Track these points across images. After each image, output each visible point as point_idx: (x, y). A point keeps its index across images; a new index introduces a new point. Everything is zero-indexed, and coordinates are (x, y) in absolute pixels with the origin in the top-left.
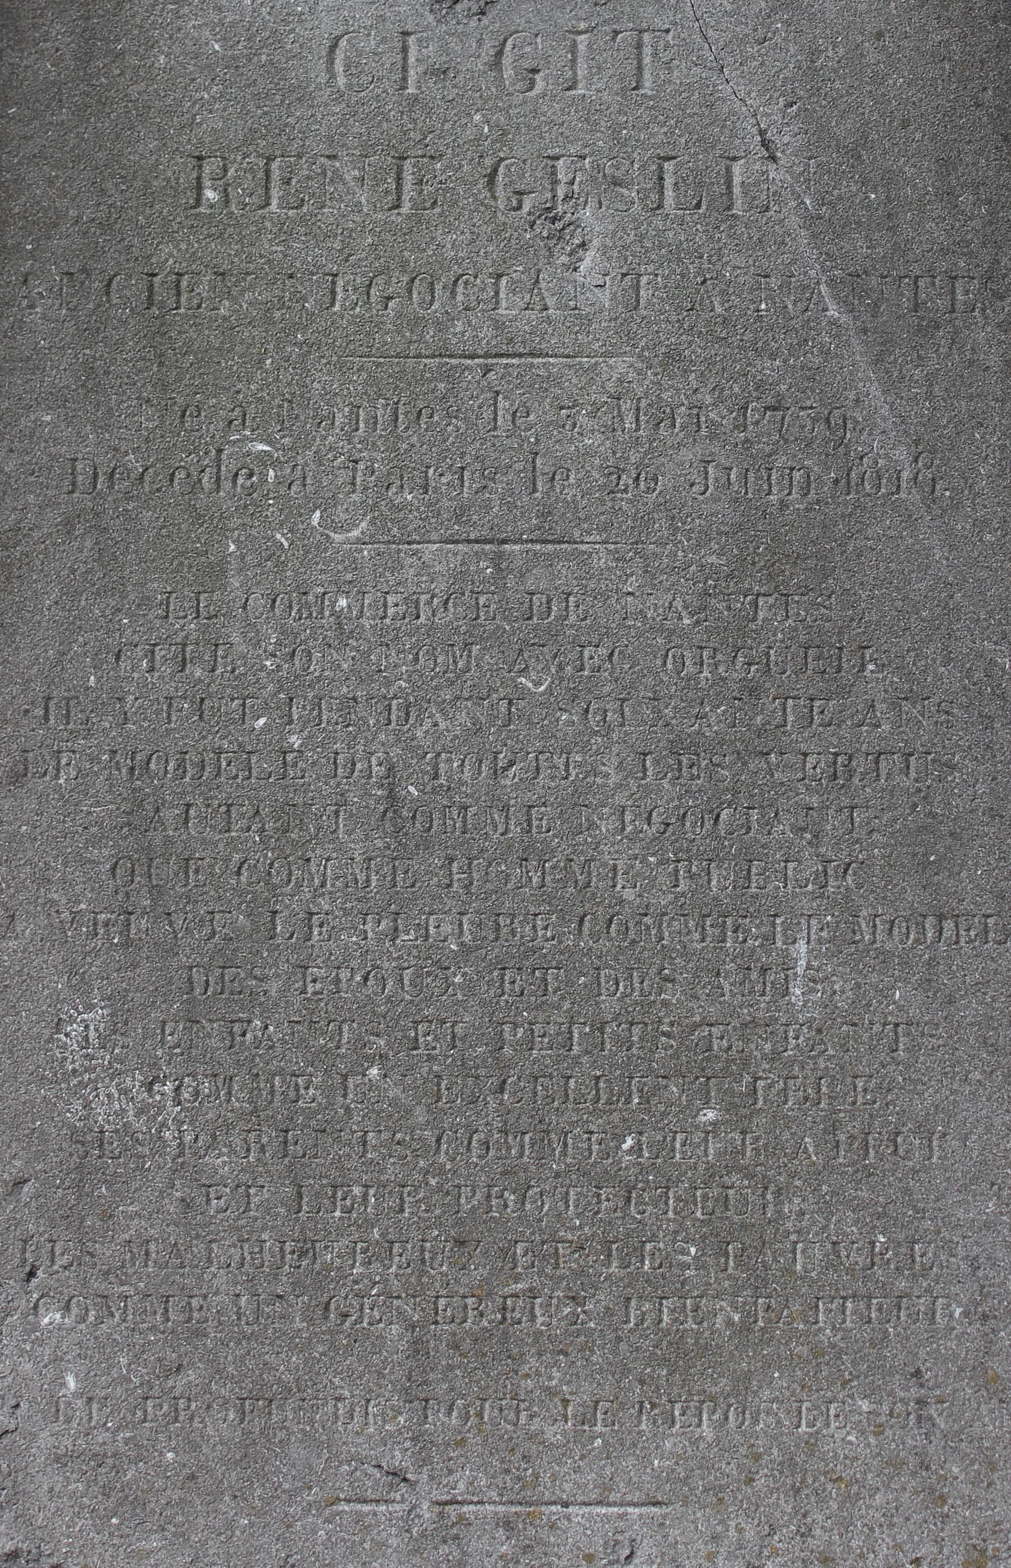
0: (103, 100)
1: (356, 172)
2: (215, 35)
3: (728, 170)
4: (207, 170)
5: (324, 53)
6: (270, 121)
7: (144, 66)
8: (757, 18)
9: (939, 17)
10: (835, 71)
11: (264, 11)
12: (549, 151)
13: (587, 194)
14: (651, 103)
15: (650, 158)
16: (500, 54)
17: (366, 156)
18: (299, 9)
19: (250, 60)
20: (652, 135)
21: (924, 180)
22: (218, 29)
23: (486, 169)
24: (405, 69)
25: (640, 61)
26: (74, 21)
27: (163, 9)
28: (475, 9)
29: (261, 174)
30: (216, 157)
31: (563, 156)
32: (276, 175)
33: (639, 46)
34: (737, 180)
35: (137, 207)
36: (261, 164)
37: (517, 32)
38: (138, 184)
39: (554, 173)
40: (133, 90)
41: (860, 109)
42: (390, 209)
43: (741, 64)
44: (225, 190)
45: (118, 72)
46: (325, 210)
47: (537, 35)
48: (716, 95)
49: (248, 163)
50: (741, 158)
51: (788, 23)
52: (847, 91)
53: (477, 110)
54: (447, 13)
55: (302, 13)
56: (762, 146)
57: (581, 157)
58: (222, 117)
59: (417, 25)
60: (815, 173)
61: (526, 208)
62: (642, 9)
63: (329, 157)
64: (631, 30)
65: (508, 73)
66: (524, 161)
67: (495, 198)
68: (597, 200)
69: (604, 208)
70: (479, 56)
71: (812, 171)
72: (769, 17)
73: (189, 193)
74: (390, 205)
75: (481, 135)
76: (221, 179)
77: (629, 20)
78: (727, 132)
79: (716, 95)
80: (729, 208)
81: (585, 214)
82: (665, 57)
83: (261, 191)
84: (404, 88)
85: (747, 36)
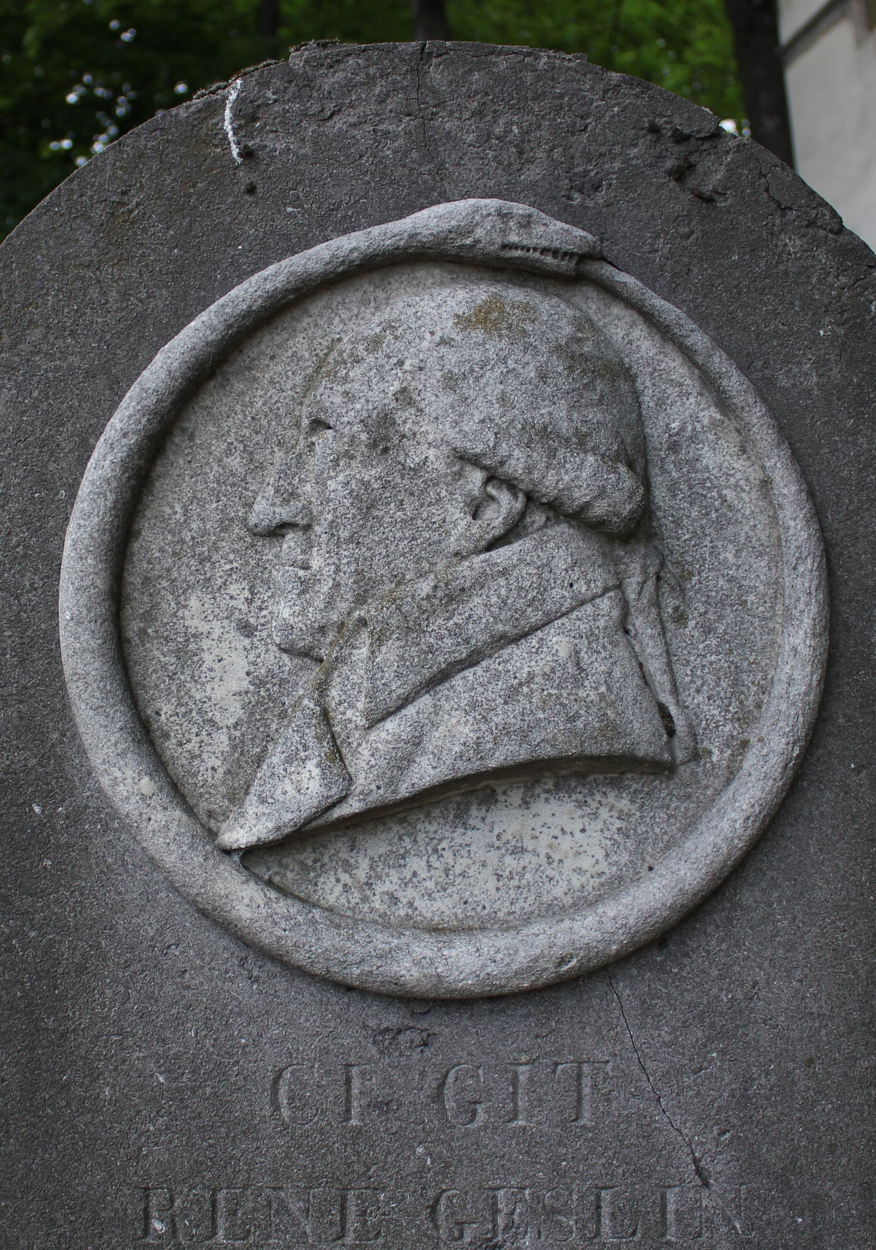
0: (50, 1131)
1: (301, 1204)
2: (160, 1067)
3: (663, 1197)
4: (154, 1201)
5: (268, 1086)
6: (216, 1153)
7: (90, 1098)
8: (694, 1047)
9: (867, 1044)
10: (768, 1099)
11: (208, 1042)
12: (490, 1183)
13: (527, 1225)
14: (590, 1135)
15: (588, 1189)
16: (442, 1085)
17: (310, 1188)
18: (243, 1041)
19: (195, 1092)
20: (592, 1166)
21: (848, 1203)
22: (162, 1061)
23: (428, 1200)
24: (348, 1101)
25: (579, 1090)
26: (19, 1051)
27: (107, 1041)
28: (417, 1040)
29: (207, 1206)
30: (163, 1188)
31: (504, 1187)
32: (222, 1205)
33: (579, 1077)
34: (671, 1207)
35: (86, 1238)
36: (208, 1196)
37: (459, 1064)
38: (86, 1215)
39: (495, 1204)
40: (79, 1121)
41: (790, 1136)
42: (334, 1240)
43: (678, 1094)
44: (173, 1220)
45: (64, 1103)
46: (271, 1241)
47: (478, 1067)
48: (653, 1126)
49: (195, 1195)
50: (676, 1186)
51: (723, 1052)
52: (778, 1119)
53: (421, 1143)
54: (390, 1044)
55: (247, 1046)
56: (696, 1174)
57: (521, 1188)
58: (168, 1150)
59: (360, 1057)
60: (745, 1199)
61: (467, 1239)
62: (582, 1042)
63: (274, 1189)
64: (571, 1062)
65: (450, 1105)
66: (466, 1193)
67: (437, 1227)
68: (536, 1232)
69: (543, 1238)
70: (422, 1089)
71: (743, 1197)
72: (705, 1046)
73: (137, 1225)
74: (334, 1236)
75: (424, 1167)
76: (168, 1210)
77: (570, 1053)
78: (662, 1161)
79: (653, 1126)
80: (663, 1235)
81: (525, 1243)
82: (605, 1088)
83: (207, 1223)
84: (348, 1119)
85: (683, 1066)
